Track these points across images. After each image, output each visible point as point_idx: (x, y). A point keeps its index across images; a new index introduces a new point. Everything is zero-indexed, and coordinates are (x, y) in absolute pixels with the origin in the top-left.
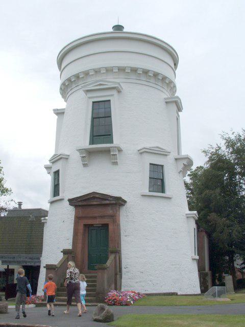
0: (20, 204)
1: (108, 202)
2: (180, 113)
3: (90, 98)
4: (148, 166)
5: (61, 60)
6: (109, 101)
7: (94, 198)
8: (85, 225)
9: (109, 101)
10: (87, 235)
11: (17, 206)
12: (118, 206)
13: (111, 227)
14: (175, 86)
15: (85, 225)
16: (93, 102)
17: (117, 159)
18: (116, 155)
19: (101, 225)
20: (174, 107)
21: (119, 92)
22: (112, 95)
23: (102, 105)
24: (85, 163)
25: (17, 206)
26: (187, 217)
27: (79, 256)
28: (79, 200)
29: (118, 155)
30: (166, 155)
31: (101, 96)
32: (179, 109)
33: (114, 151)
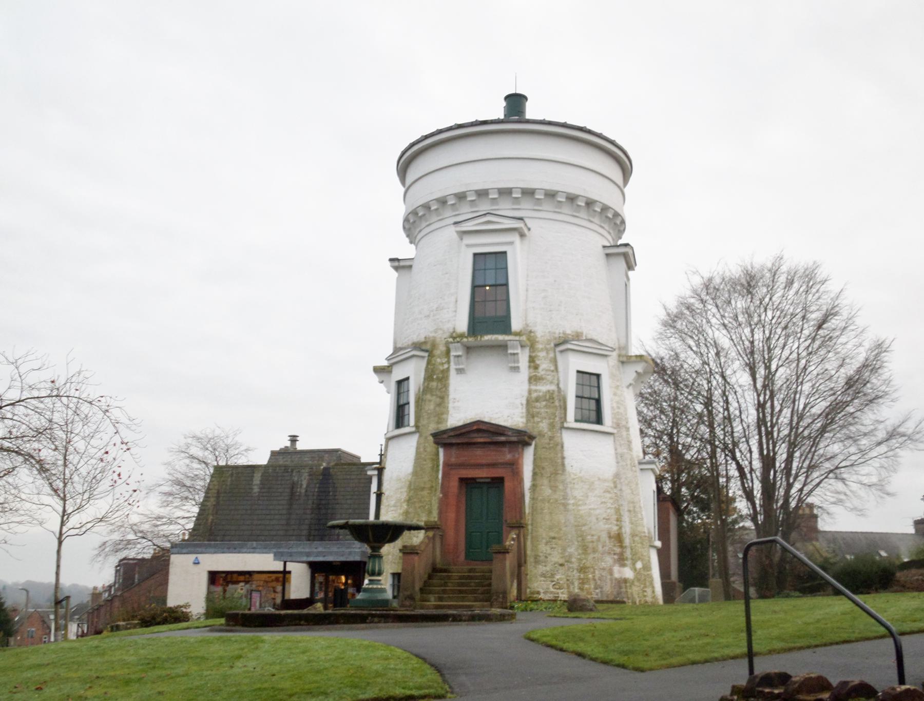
0: (294, 439)
1: (503, 439)
2: (630, 273)
3: (468, 246)
4: (575, 374)
5: (405, 164)
6: (505, 253)
7: (479, 431)
8: (462, 480)
9: (505, 253)
10: (463, 500)
11: (288, 444)
12: (520, 446)
13: (508, 484)
14: (623, 222)
15: (462, 480)
16: (475, 255)
17: (518, 361)
18: (517, 354)
19: (489, 480)
20: (622, 264)
21: (522, 235)
22: (511, 243)
23: (490, 263)
24: (461, 367)
25: (288, 444)
26: (608, 255)
27: (451, 533)
28: (452, 434)
29: (520, 355)
30: (606, 356)
31: (488, 244)
32: (630, 266)
33: (514, 347)
